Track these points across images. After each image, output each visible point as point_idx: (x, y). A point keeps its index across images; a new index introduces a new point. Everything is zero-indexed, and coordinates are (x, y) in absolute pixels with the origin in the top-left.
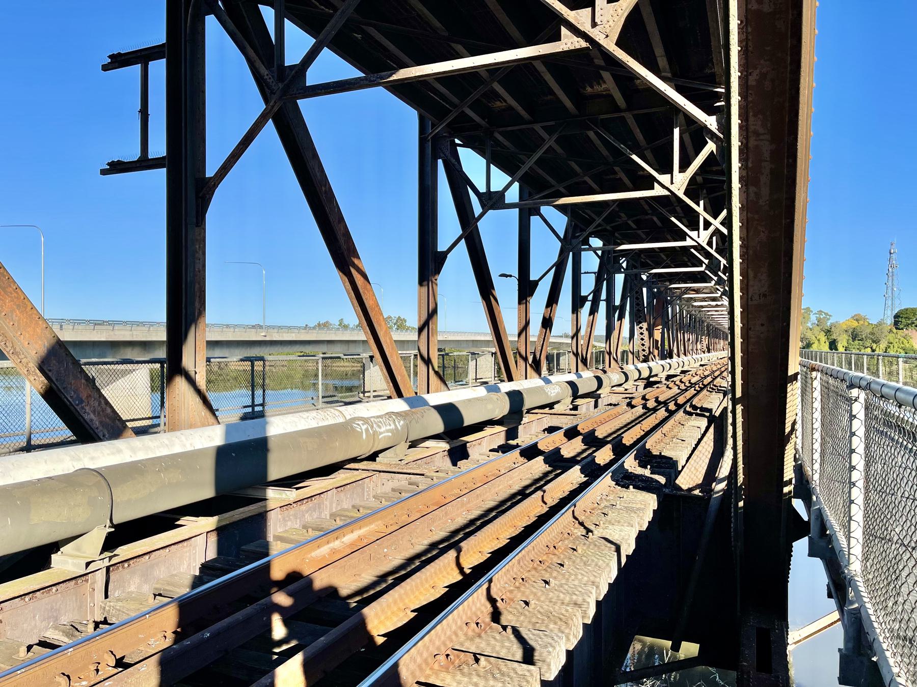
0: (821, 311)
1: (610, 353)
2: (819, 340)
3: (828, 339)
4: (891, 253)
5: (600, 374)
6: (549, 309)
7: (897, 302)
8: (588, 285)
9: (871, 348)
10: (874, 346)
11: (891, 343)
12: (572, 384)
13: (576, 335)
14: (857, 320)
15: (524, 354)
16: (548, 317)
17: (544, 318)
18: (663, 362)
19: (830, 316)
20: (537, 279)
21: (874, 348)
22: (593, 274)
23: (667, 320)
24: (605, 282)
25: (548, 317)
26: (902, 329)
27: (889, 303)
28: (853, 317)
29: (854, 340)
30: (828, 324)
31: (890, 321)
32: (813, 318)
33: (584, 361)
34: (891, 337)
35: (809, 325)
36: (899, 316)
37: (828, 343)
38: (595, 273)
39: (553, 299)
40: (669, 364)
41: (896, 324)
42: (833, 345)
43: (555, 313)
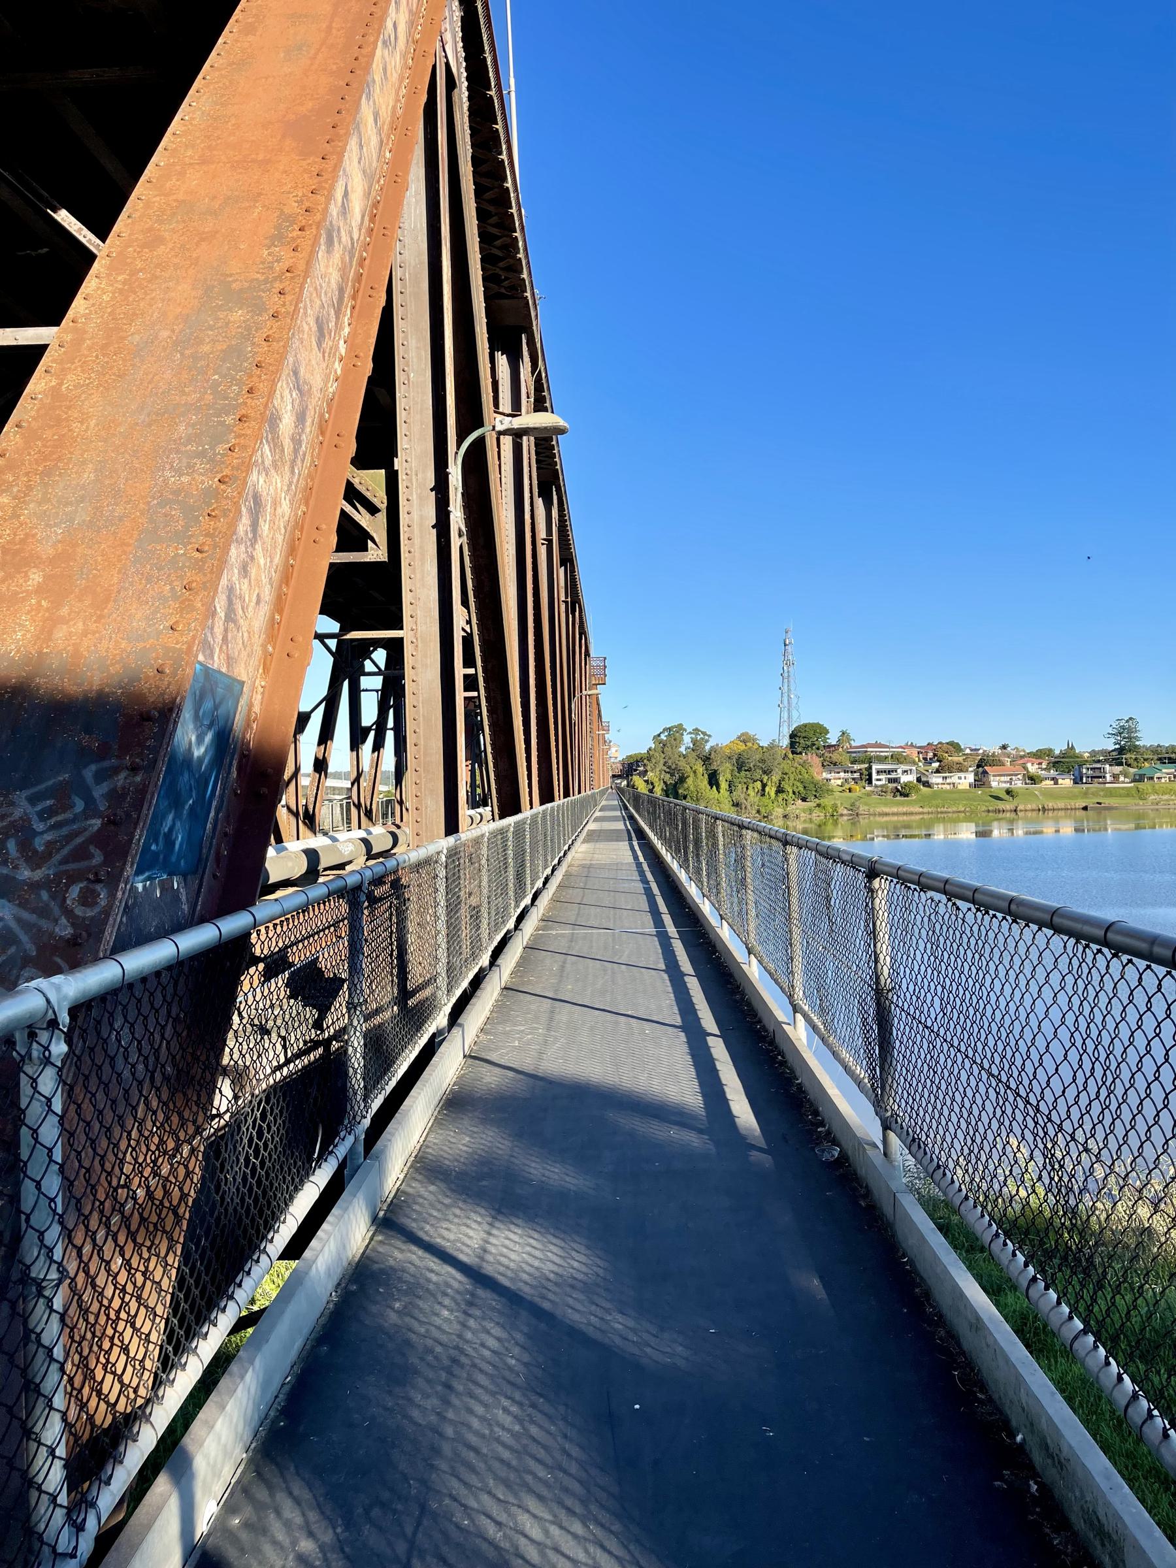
0: (697, 730)
1: (401, 803)
2: (695, 772)
3: (707, 770)
4: (785, 645)
5: (394, 829)
6: (322, 747)
7: (795, 714)
8: (369, 716)
9: (762, 781)
10: (765, 778)
11: (786, 774)
12: (365, 841)
13: (357, 780)
14: (745, 742)
15: (294, 809)
16: (321, 758)
17: (316, 759)
18: (472, 812)
19: (709, 736)
20: (309, 710)
21: (765, 781)
22: (375, 693)
23: (478, 752)
24: (391, 711)
25: (321, 758)
26: (801, 753)
27: (785, 715)
28: (739, 738)
29: (739, 770)
30: (707, 748)
31: (785, 742)
32: (687, 739)
33: (369, 813)
34: (786, 765)
35: (682, 749)
36: (796, 736)
37: (706, 776)
38: (377, 691)
39: (326, 734)
40: (481, 814)
41: (792, 745)
42: (713, 780)
43: (329, 754)
